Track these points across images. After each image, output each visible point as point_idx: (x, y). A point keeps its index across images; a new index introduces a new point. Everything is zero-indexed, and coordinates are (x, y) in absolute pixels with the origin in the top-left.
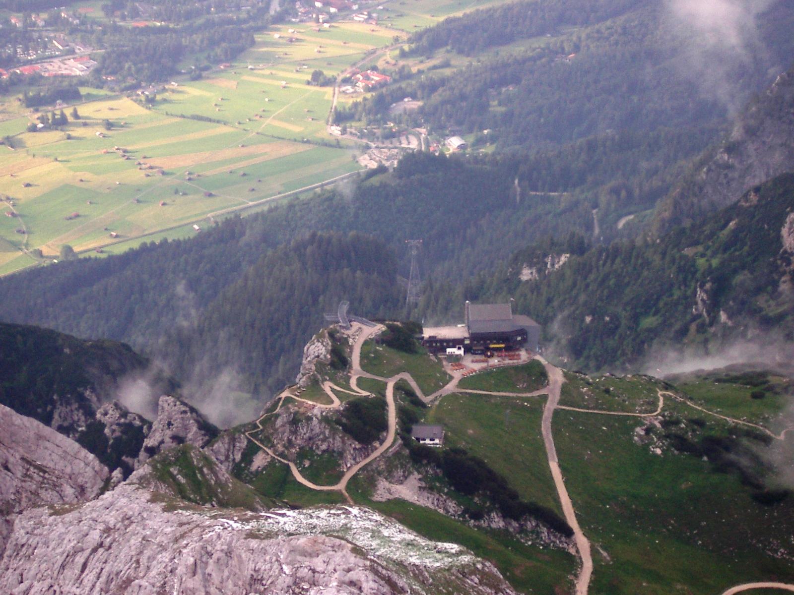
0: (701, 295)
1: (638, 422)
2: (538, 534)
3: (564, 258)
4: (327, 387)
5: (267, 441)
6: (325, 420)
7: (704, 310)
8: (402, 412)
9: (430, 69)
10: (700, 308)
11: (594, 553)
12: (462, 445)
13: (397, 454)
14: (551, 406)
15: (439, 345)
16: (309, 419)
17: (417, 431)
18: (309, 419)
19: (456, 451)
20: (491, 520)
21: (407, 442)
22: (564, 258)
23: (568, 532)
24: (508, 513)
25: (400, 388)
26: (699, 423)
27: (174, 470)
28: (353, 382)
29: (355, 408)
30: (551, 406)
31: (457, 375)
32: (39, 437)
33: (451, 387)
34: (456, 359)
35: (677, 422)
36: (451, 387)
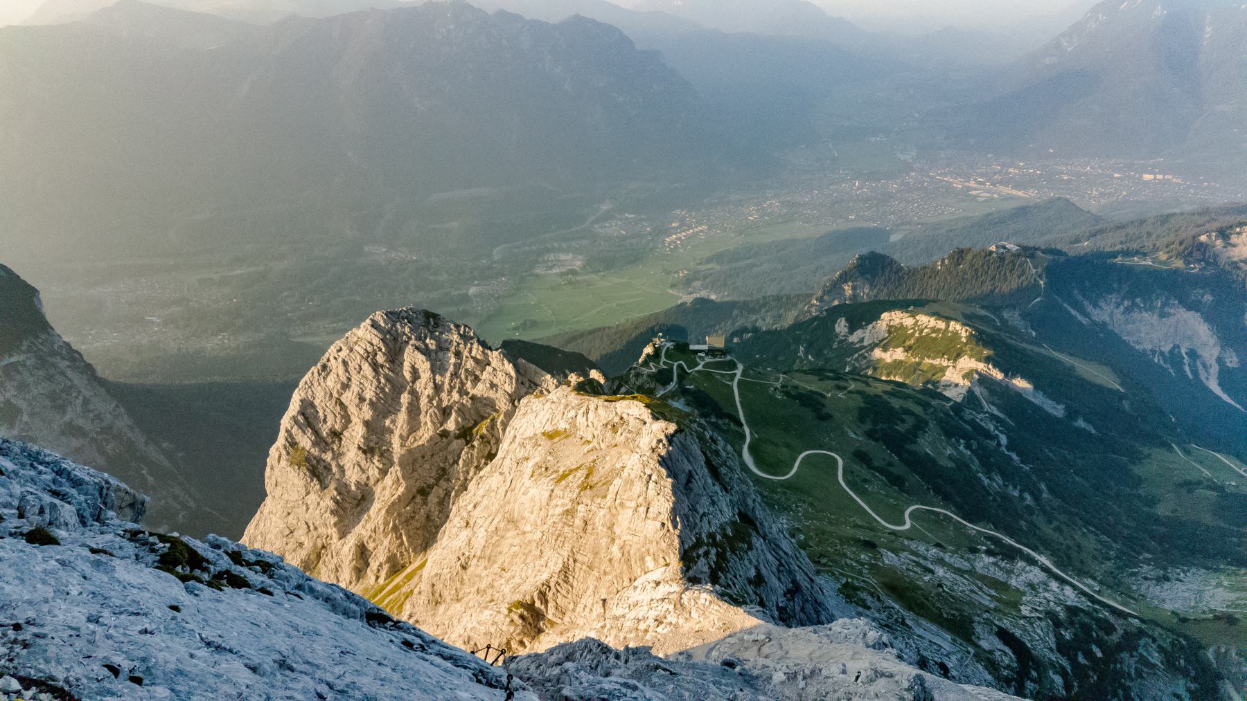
0: (802, 348)
1: (771, 385)
2: (730, 425)
3: (750, 335)
4: (651, 364)
5: (626, 383)
6: (649, 376)
7: (1215, 666)
8: (679, 375)
9: (415, 395)
10: (801, 354)
11: (751, 433)
12: (702, 389)
13: (676, 391)
14: (738, 377)
15: (697, 352)
16: (643, 375)
17: (685, 382)
18: (643, 375)
19: (700, 391)
20: (711, 418)
21: (680, 387)
22: (750, 335)
23: (741, 425)
24: (718, 416)
25: (680, 366)
26: (796, 387)
27: (587, 387)
28: (661, 364)
29: (661, 372)
30: (738, 377)
31: (702, 363)
32: (536, 372)
33: (699, 368)
34: (701, 358)
35: (787, 387)
36: (699, 368)
